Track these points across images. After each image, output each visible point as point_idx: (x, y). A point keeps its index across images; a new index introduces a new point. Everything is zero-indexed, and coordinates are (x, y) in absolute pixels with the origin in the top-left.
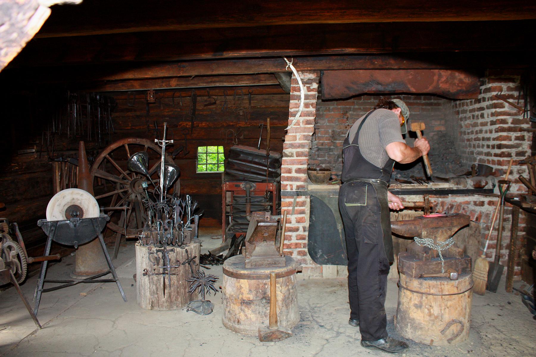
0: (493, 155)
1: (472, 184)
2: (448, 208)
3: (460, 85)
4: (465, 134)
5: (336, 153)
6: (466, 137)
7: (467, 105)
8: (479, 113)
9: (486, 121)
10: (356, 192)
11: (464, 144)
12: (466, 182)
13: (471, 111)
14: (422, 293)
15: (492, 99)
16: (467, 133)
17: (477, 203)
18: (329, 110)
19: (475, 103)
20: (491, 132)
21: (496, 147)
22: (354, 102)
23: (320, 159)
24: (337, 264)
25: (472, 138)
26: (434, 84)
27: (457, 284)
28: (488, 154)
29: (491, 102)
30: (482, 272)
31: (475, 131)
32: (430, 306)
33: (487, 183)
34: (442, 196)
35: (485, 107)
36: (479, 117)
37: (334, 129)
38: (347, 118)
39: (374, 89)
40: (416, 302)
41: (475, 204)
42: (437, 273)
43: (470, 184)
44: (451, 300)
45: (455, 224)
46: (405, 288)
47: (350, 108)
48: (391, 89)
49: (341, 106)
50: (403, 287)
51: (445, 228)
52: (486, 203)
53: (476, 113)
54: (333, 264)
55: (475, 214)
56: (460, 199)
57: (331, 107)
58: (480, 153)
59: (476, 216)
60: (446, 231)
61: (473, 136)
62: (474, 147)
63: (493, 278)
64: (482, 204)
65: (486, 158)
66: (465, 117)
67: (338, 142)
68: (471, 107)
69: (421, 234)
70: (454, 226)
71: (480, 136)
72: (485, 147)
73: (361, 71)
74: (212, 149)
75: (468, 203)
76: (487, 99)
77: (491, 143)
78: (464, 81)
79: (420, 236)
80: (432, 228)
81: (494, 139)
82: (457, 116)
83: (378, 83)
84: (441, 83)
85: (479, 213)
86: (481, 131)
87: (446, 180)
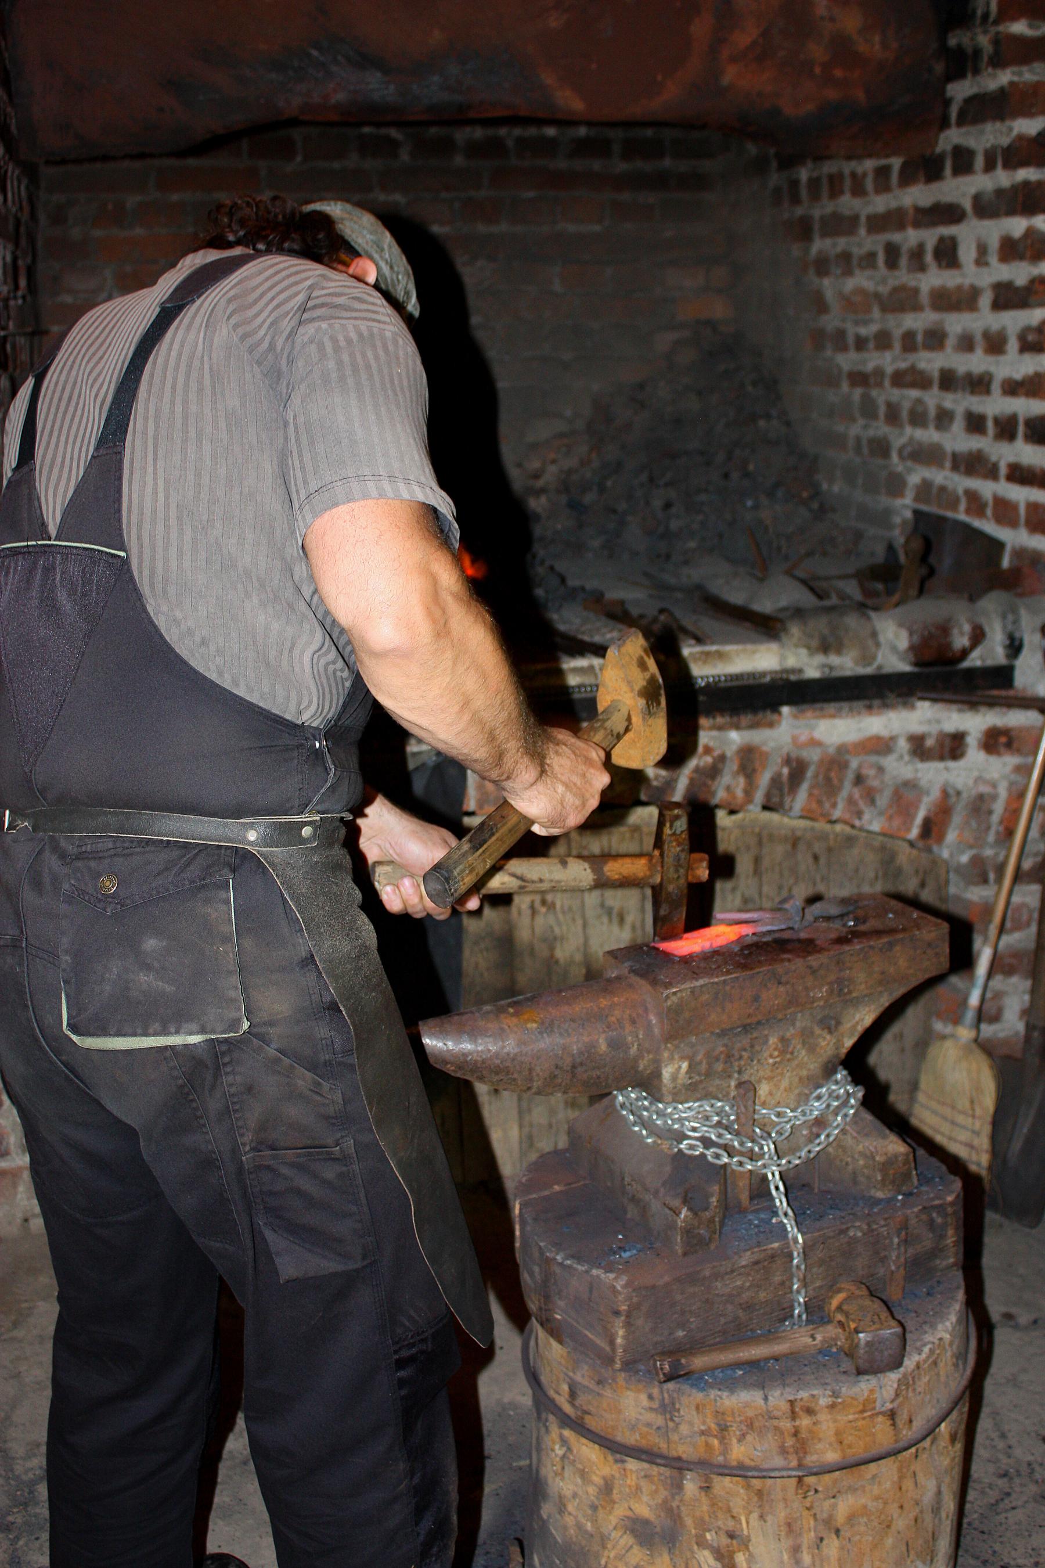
0: (1003, 471)
1: (903, 642)
3: (838, 73)
4: (844, 348)
6: (847, 361)
7: (858, 190)
8: (930, 237)
9: (967, 282)
10: (151, 944)
11: (832, 397)
12: (874, 634)
13: (879, 223)
14: (679, 1465)
15: (1014, 155)
16: (851, 340)
17: (929, 743)
19: (907, 178)
20: (995, 344)
21: (1021, 429)
25: (879, 372)
27: (888, 1392)
28: (973, 464)
29: (1004, 178)
30: (960, 1119)
31: (897, 333)
32: (731, 1536)
33: (978, 636)
34: (746, 719)
35: (967, 205)
36: (929, 258)
39: (340, 97)
40: (643, 1509)
41: (919, 748)
43: (890, 642)
44: (852, 1489)
46: (566, 1421)
50: (557, 1411)
51: (802, 1021)
53: (911, 237)
55: (915, 805)
56: (838, 729)
57: (132, 201)
58: (929, 455)
59: (921, 815)
60: (806, 1035)
61: (889, 361)
62: (893, 416)
63: (1017, 1145)
64: (953, 746)
65: (962, 483)
66: (846, 257)
68: (880, 204)
69: (658, 1075)
71: (931, 362)
72: (958, 425)
75: (882, 746)
76: (979, 162)
77: (996, 405)
78: (862, 48)
79: (649, 1084)
80: (723, 1033)
81: (1012, 388)
82: (796, 250)
83: (365, 61)
85: (935, 794)
86: (935, 339)
87: (767, 627)
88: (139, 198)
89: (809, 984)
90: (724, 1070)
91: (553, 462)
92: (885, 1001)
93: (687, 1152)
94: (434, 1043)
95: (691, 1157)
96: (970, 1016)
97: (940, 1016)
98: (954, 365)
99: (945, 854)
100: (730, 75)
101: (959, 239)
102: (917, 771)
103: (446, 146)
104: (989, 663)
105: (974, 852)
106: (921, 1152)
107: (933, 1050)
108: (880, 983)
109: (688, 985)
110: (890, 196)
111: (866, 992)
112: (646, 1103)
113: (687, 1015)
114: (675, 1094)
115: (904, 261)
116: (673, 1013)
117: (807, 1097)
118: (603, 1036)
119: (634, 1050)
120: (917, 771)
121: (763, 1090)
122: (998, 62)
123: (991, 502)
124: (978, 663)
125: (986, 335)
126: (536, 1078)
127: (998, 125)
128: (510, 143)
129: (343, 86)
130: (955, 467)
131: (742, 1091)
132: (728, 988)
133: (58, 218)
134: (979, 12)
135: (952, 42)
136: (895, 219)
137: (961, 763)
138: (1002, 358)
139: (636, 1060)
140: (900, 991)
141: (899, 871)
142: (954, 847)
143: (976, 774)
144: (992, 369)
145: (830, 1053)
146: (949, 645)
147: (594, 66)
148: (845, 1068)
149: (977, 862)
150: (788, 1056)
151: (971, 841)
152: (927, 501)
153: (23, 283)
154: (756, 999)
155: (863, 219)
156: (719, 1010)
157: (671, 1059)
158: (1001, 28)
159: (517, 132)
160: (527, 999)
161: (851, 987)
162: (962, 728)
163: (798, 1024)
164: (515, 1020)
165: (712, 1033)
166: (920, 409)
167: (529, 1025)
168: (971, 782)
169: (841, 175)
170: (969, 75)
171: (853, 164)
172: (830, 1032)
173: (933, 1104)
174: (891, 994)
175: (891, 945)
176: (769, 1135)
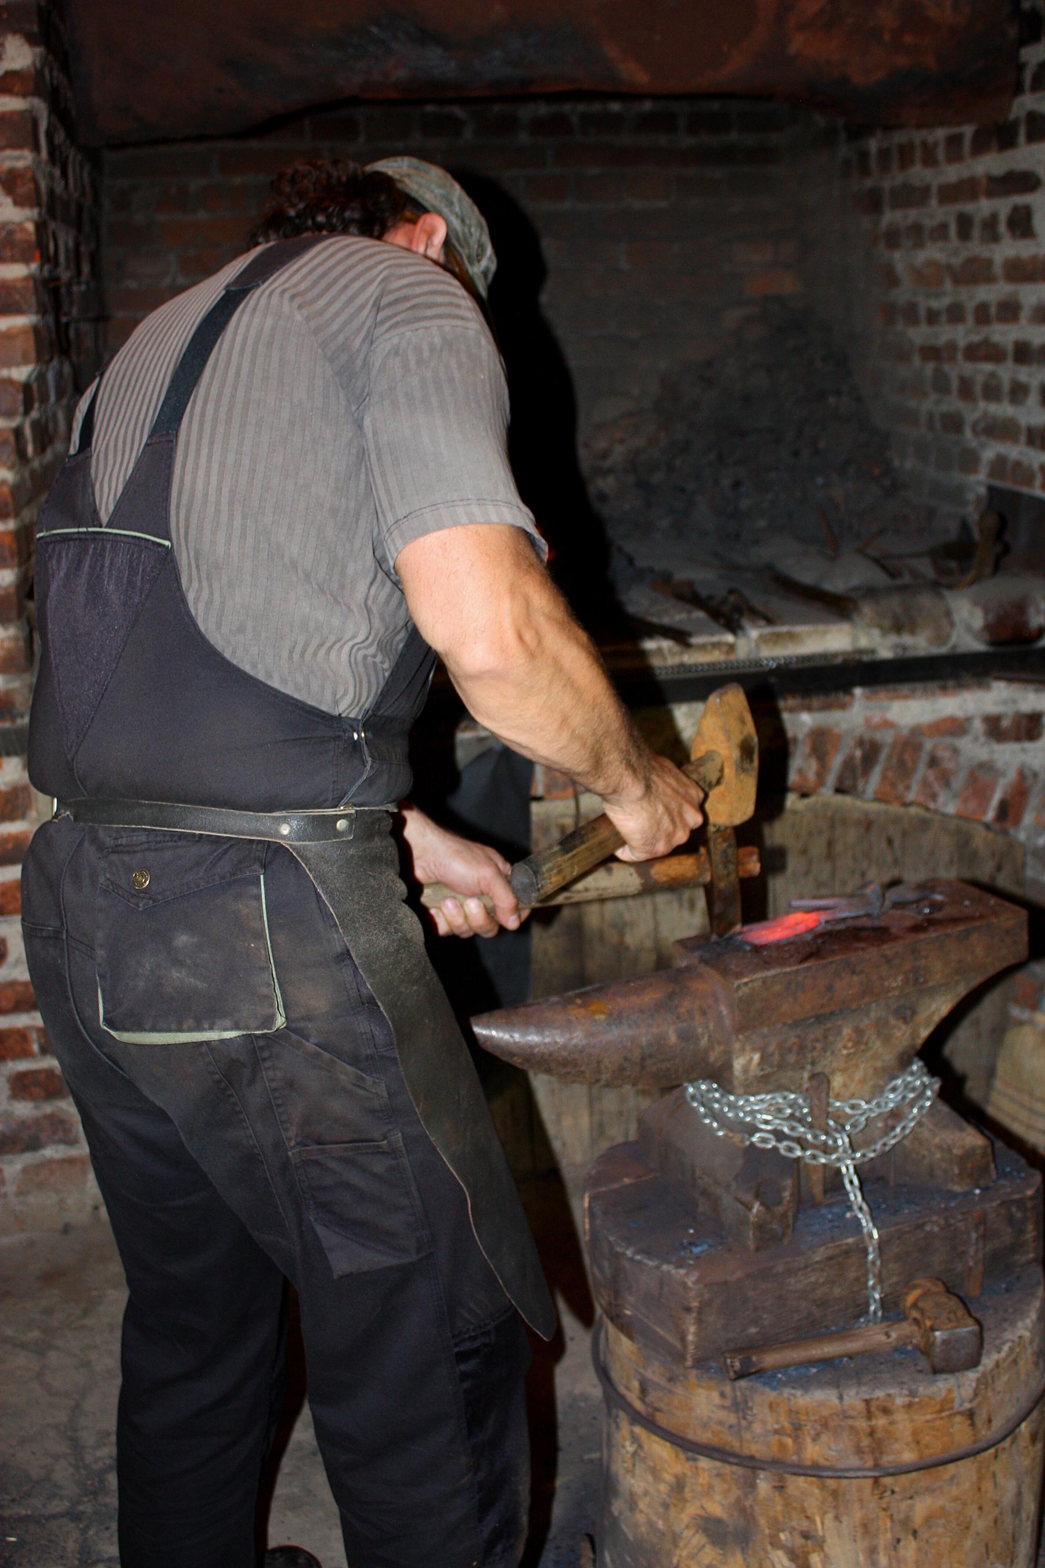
1: (978, 621)
2: (848, 764)
3: (908, 39)
6: (918, 335)
7: (930, 160)
8: (1003, 206)
12: (948, 614)
13: (950, 193)
14: (751, 1464)
16: (922, 313)
17: (1005, 723)
19: (980, 147)
25: (952, 346)
27: (967, 1391)
31: (970, 306)
32: (806, 1536)
34: (816, 702)
36: (1002, 228)
39: (401, 74)
40: (716, 1508)
42: (843, 1333)
43: (965, 621)
44: (930, 1490)
46: (637, 1418)
51: (876, 1011)
53: (984, 207)
55: (990, 788)
56: (911, 710)
57: (195, 184)
58: (1004, 430)
60: (881, 1026)
61: (962, 334)
62: (966, 390)
66: (917, 229)
68: (951, 173)
69: (728, 1066)
70: (931, 992)
71: (1005, 335)
75: (956, 727)
79: (720, 1075)
85: (1011, 775)
86: (1009, 311)
87: (839, 607)
90: (796, 1062)
94: (501, 1035)
97: (1016, 1001)
99: (1022, 836)
106: (999, 1144)
109: (759, 975)
112: (717, 1095)
115: (976, 232)
116: (745, 1004)
119: (704, 1042)
128: (575, 120)
130: (1030, 442)
131: (814, 1083)
132: (800, 978)
136: (968, 189)
139: (706, 1051)
141: (974, 854)
146: (1025, 624)
153: (86, 269)
154: (829, 988)
155: (934, 190)
157: (743, 1050)
163: (873, 1015)
164: (582, 1011)
165: (784, 1024)
167: (597, 1017)
169: (911, 146)
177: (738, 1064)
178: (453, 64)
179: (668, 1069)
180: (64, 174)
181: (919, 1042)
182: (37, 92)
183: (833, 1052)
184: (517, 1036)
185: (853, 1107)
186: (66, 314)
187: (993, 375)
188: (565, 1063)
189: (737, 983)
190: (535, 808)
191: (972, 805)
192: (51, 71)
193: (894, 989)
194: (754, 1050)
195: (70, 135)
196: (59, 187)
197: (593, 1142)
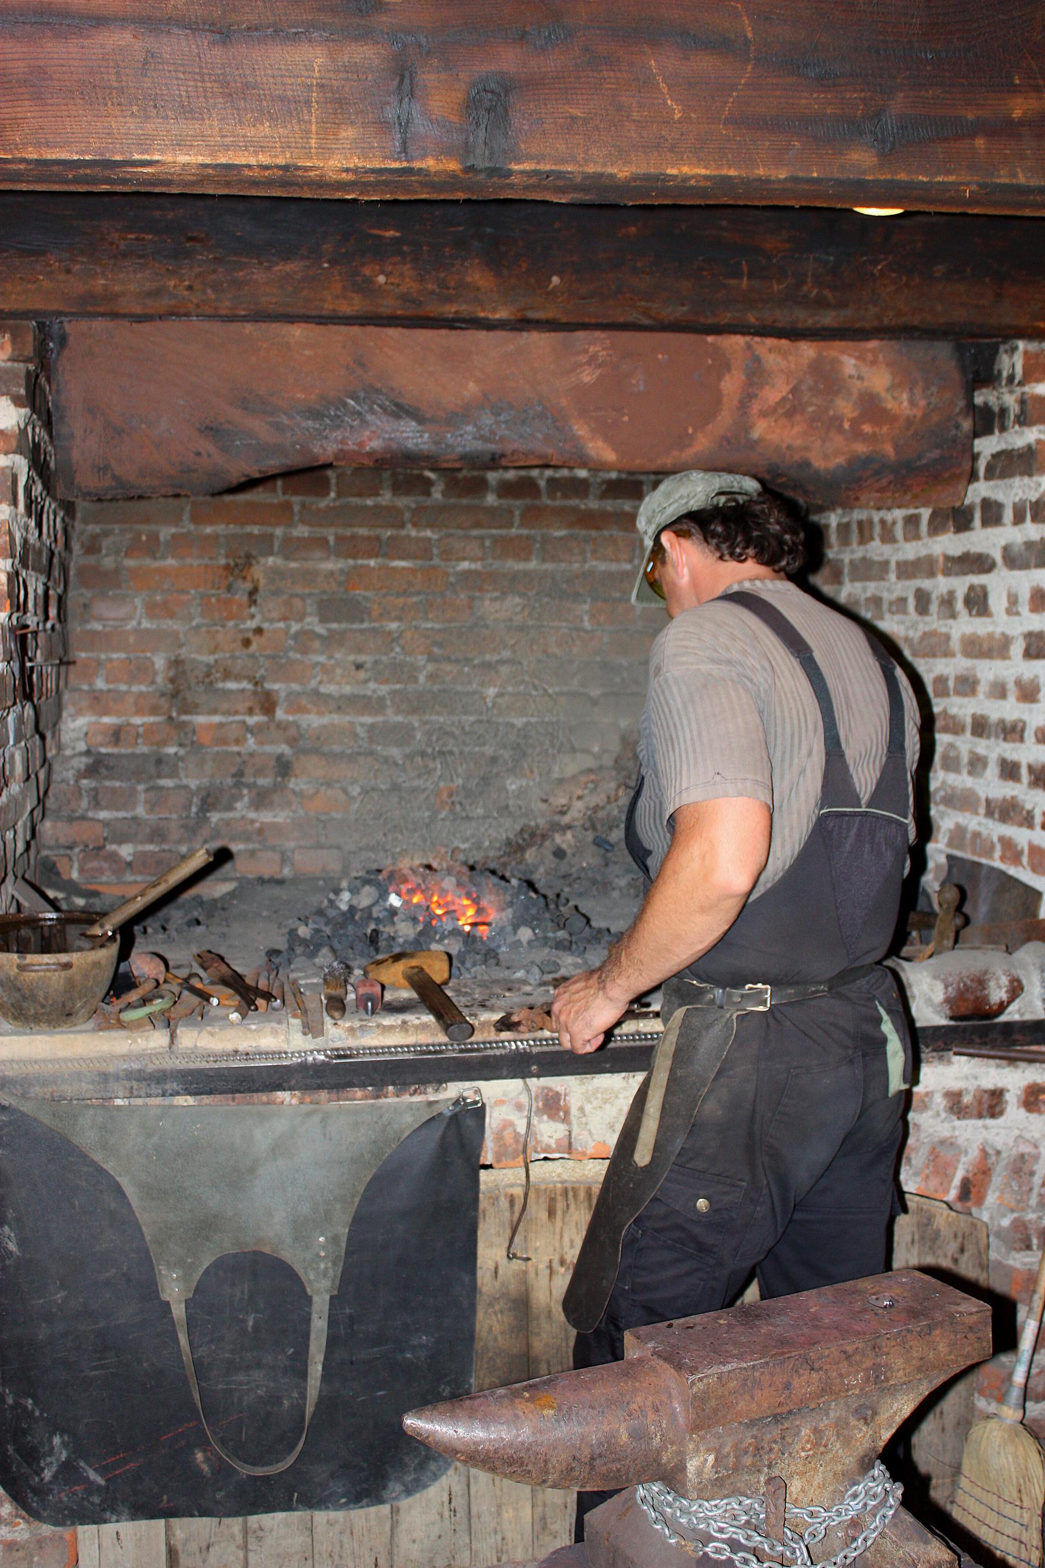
1: (939, 995)
3: (867, 428)
5: (193, 784)
7: (888, 537)
8: (961, 585)
9: (999, 630)
13: (908, 570)
17: (967, 1099)
18: (152, 547)
19: (936, 527)
22: (287, 507)
23: (103, 815)
24: (169, 1513)
26: (725, 419)
28: (1006, 811)
30: (1007, 1510)
33: (1016, 989)
35: (998, 556)
36: (959, 605)
37: (183, 652)
38: (253, 592)
39: (376, 444)
45: (899, 1376)
47: (267, 540)
48: (479, 446)
49: (220, 529)
51: (836, 1411)
52: (1012, 1099)
53: (940, 585)
54: (144, 1510)
57: (166, 532)
59: (959, 1175)
60: (841, 1427)
64: (992, 1103)
65: (995, 830)
67: (201, 719)
68: (910, 551)
70: (892, 1391)
72: (992, 771)
73: (297, 332)
74: (939, 267)
76: (1008, 515)
78: (890, 405)
79: (672, 1478)
80: (753, 1423)
83: (401, 410)
84: (763, 414)
85: (974, 1153)
88: (173, 530)
89: (844, 1371)
90: (753, 1465)
91: (580, 798)
92: (925, 1390)
93: (712, 1555)
94: (444, 1429)
95: (716, 1561)
96: (1015, 1394)
97: (982, 1393)
98: (985, 712)
99: (985, 1217)
100: (760, 429)
101: (989, 588)
102: (954, 1128)
103: (478, 486)
104: (1028, 1017)
105: (1016, 1215)
106: (966, 1558)
107: (976, 1431)
108: (919, 1370)
109: (716, 1369)
110: (920, 543)
111: (905, 1379)
112: (670, 1498)
113: (713, 1403)
114: (700, 1490)
115: (934, 607)
116: (699, 1401)
117: (843, 1494)
118: (623, 1425)
119: (656, 1441)
120: (954, 1128)
121: (795, 1486)
122: (1024, 420)
123: (1026, 852)
124: (1017, 1017)
125: (1018, 683)
126: (552, 1471)
127: (1026, 479)
128: (542, 484)
129: (379, 434)
130: (989, 814)
131: (772, 1488)
132: (757, 1374)
133: (92, 548)
134: (1005, 374)
135: (979, 399)
136: (924, 567)
137: (1000, 1121)
138: (1034, 706)
139: (658, 1452)
140: (943, 1378)
141: (936, 1235)
142: (994, 1210)
143: (1017, 1132)
144: (1025, 717)
145: (866, 1445)
146: (985, 999)
147: (626, 419)
148: (883, 1463)
149: (1019, 1225)
150: (822, 1449)
151: (1013, 1204)
152: (961, 847)
153: (53, 612)
154: (787, 1386)
155: (893, 565)
156: (747, 1397)
157: (697, 1450)
158: (1026, 389)
159: (548, 473)
160: (544, 1382)
161: (888, 1374)
162: (1000, 1085)
163: (832, 1414)
164: (531, 1406)
165: (740, 1423)
166: (952, 754)
167: (545, 1412)
168: (1011, 1142)
169: (871, 522)
170: (996, 431)
171: (882, 513)
172: (866, 1424)
173: (977, 1491)
174: (930, 1382)
175: (930, 1328)
176: (802, 1537)
177: (692, 1466)
178: (426, 435)
179: (618, 1470)
180: (39, 525)
181: (882, 1444)
182: (19, 451)
183: (790, 1454)
184: (461, 1431)
185: (812, 1514)
186: (30, 660)
187: (951, 746)
188: (511, 1461)
189: (691, 1378)
190: (483, 1174)
191: (933, 1183)
192: (34, 429)
193: (854, 1387)
194: (708, 1450)
195: (47, 487)
196: (33, 539)
197: (536, 1537)
